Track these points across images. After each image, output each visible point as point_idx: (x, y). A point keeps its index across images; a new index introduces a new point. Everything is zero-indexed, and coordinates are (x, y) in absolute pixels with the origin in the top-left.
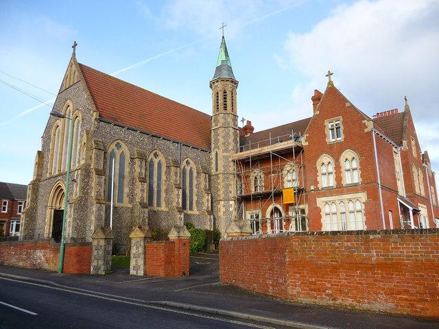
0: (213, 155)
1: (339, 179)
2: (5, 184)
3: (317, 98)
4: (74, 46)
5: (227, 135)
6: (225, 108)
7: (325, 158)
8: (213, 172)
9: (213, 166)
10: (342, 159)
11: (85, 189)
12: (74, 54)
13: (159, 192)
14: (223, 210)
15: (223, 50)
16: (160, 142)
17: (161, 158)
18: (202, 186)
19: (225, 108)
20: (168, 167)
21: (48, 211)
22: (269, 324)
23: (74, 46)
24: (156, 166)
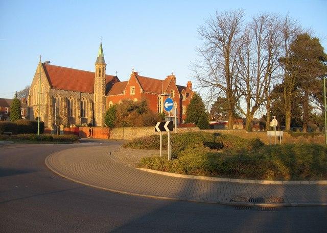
0: (95, 94)
2: (4, 99)
4: (40, 57)
5: (100, 87)
6: (100, 76)
8: (94, 102)
9: (94, 99)
13: (72, 104)
15: (100, 49)
16: (72, 92)
17: (73, 98)
18: (89, 107)
19: (100, 76)
20: (75, 102)
22: (59, 172)
23: (40, 57)
24: (71, 102)
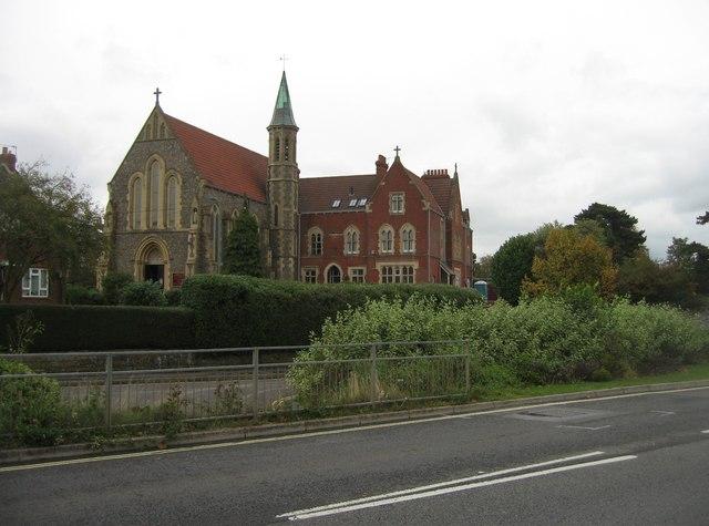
1: (397, 248)
3: (381, 163)
4: (158, 93)
7: (388, 228)
10: (401, 231)
11: (202, 251)
12: (157, 102)
14: (283, 266)
21: (136, 266)
23: (158, 93)
